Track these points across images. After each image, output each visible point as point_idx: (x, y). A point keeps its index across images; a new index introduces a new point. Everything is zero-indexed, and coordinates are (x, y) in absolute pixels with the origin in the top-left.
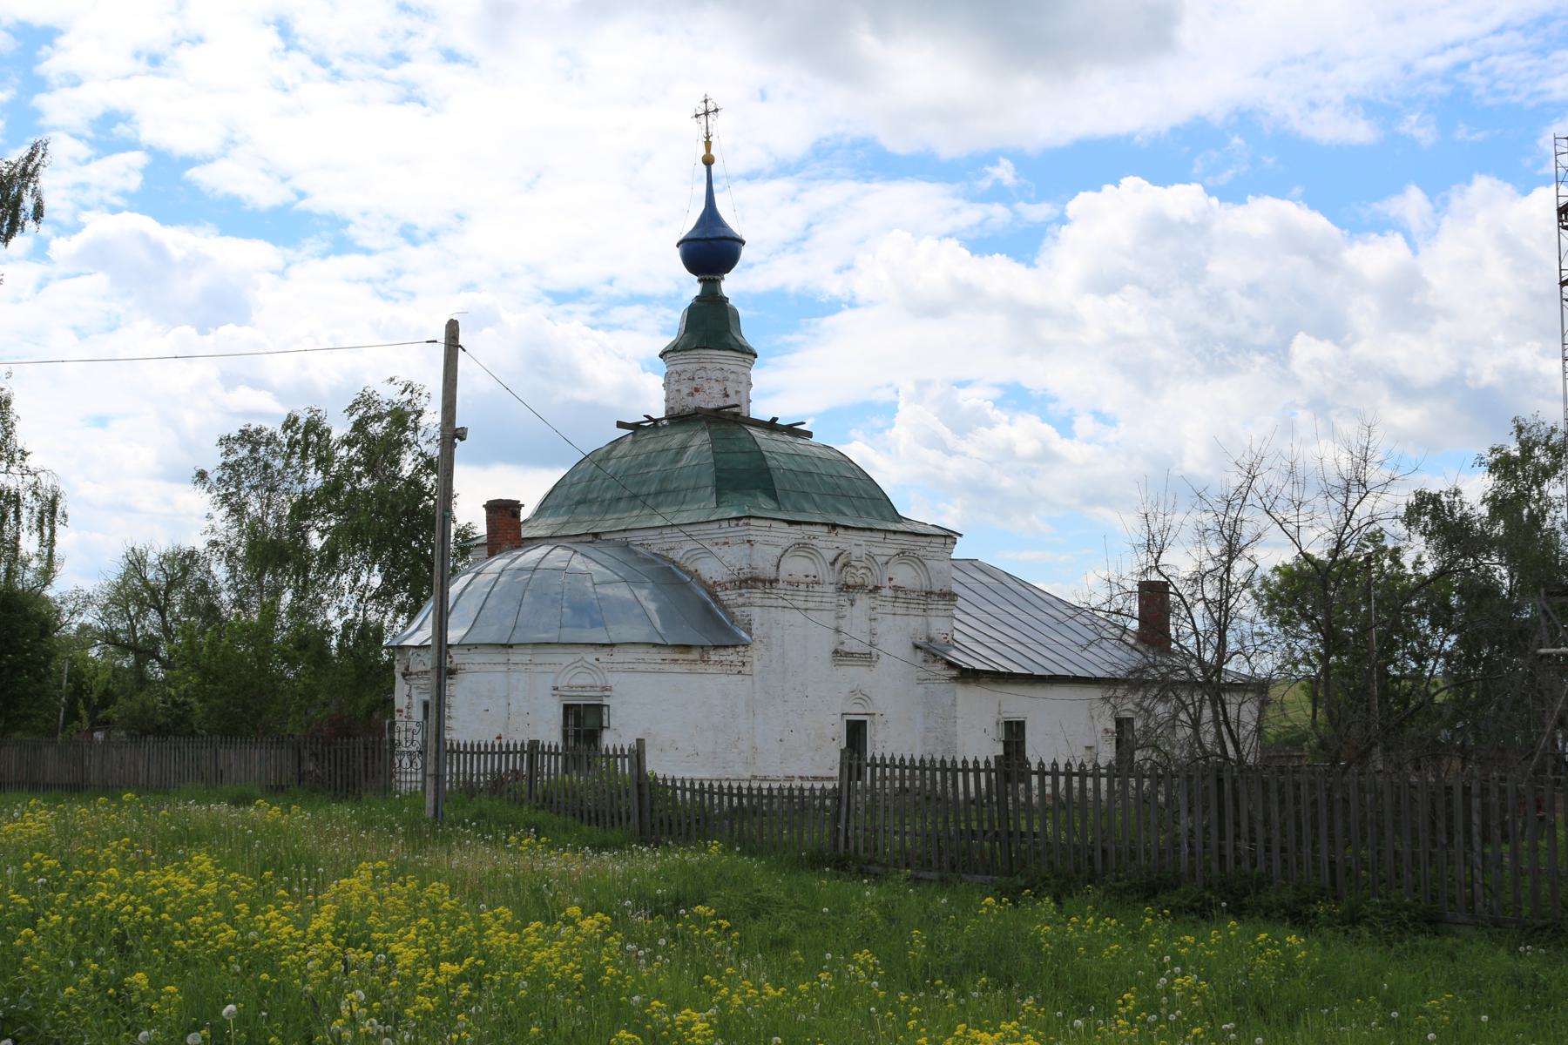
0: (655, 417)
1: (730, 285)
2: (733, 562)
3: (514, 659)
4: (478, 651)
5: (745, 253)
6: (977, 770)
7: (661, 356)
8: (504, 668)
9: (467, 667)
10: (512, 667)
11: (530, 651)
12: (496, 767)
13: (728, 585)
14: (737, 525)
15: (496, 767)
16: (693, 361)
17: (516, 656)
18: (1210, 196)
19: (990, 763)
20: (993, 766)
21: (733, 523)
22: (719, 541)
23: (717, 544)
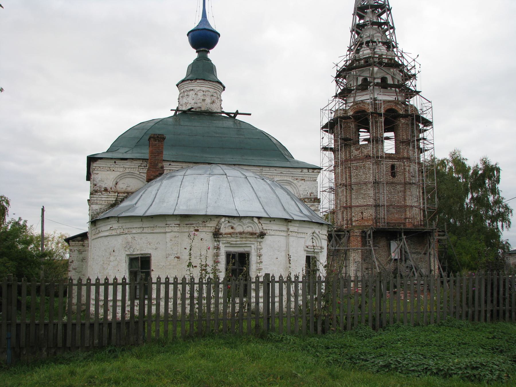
0: (404, 63)
1: (213, 55)
2: (307, 189)
3: (292, 229)
4: (275, 222)
5: (220, 40)
6: (296, 282)
7: (177, 85)
8: (284, 234)
9: (268, 231)
10: (291, 233)
11: (298, 225)
12: (284, 304)
13: (306, 200)
14: (313, 172)
15: (284, 304)
16: (213, 87)
17: (293, 228)
18: (367, 89)
19: (125, 279)
20: (128, 281)
21: (311, 171)
22: (298, 178)
23: (297, 179)
